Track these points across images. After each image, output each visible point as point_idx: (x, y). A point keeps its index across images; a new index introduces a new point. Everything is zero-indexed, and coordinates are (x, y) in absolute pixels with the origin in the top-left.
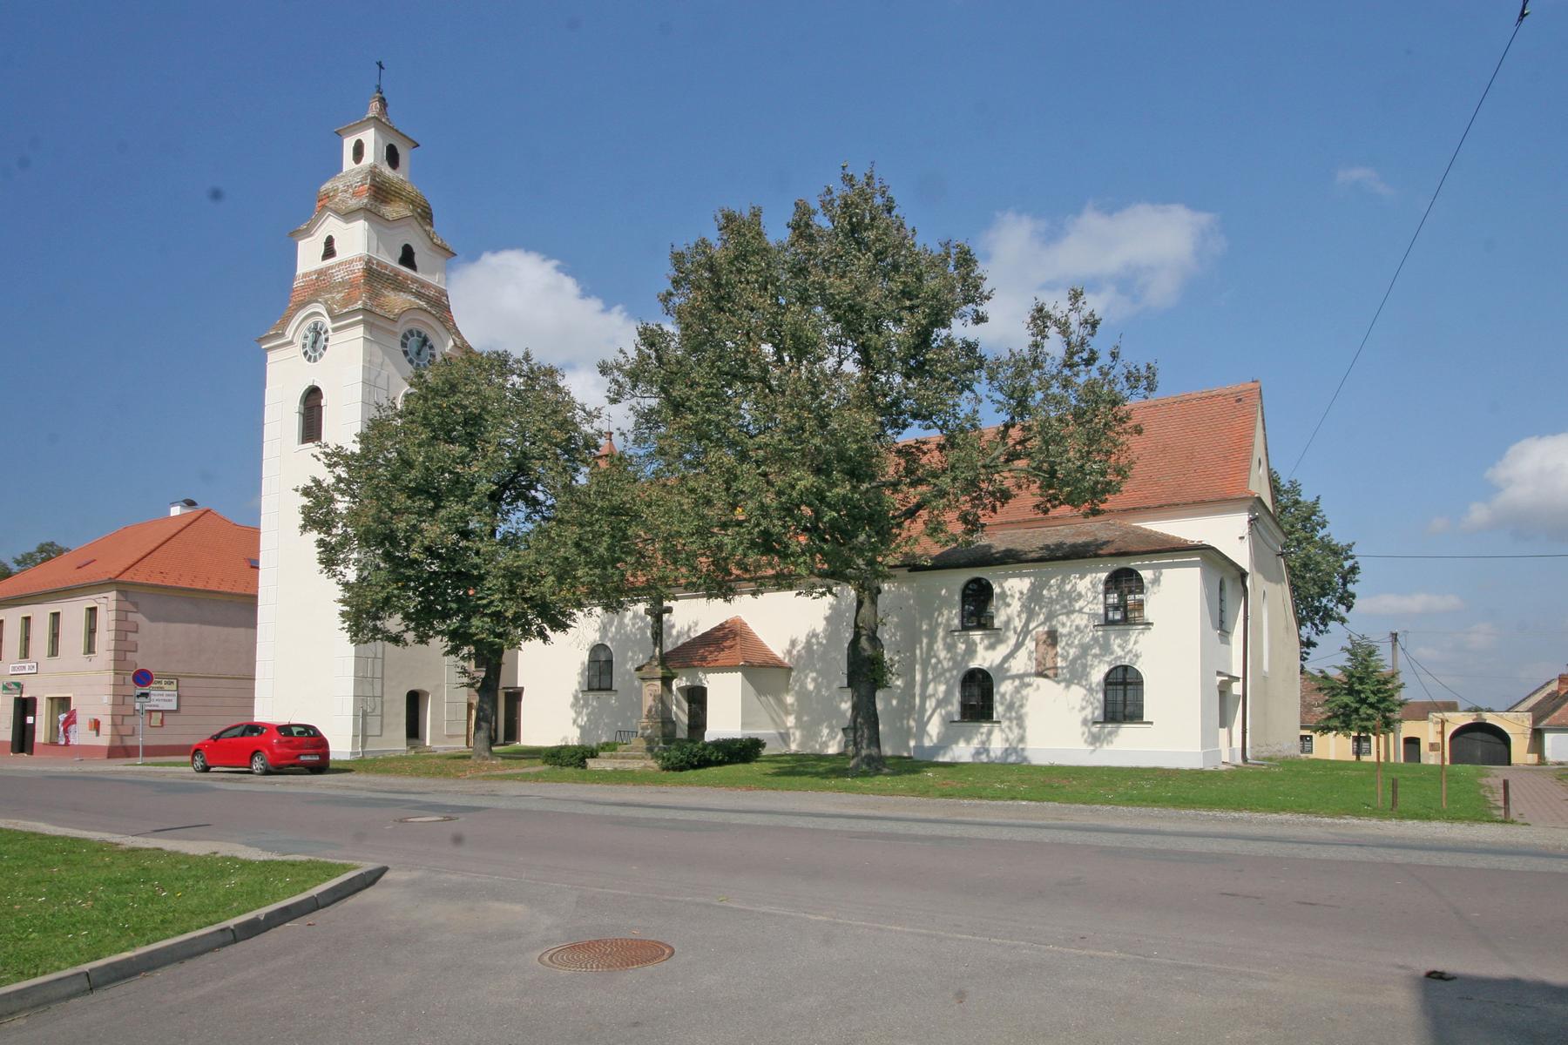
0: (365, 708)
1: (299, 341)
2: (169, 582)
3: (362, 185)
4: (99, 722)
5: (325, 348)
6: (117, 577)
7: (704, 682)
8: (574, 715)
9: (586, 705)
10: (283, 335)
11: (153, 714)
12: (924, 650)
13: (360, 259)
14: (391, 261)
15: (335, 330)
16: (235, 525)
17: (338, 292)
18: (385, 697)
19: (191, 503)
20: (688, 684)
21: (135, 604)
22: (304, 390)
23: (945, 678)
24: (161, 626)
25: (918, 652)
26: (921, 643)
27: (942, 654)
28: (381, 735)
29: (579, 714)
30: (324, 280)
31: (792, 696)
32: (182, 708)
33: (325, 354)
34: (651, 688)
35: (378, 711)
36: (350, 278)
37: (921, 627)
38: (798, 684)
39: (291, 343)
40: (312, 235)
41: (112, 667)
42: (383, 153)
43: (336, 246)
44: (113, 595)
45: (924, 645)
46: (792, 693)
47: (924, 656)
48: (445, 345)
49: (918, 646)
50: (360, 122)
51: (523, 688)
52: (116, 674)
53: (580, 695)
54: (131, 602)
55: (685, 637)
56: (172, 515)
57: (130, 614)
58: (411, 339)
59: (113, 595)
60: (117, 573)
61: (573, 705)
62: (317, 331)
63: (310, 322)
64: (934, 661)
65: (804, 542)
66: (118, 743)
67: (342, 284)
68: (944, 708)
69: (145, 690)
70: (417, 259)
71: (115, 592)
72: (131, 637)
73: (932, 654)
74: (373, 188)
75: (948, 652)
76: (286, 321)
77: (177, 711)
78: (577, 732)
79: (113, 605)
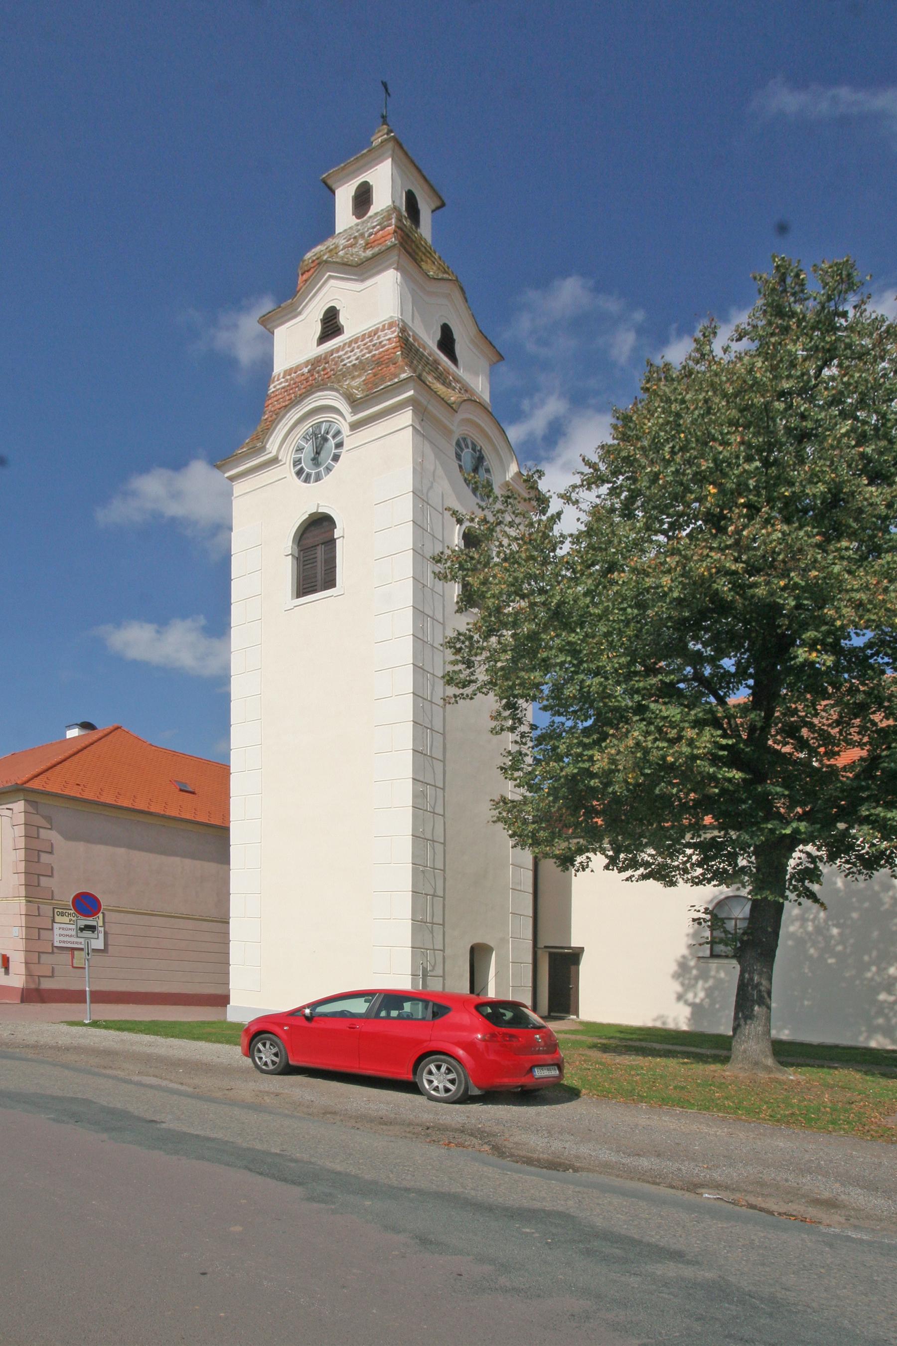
0: (425, 965)
1: (287, 457)
2: (89, 795)
3: (382, 229)
4: (8, 959)
5: (336, 458)
6: (25, 783)
8: (679, 988)
9: (704, 975)
10: (263, 449)
11: (76, 952)
13: (391, 325)
14: (430, 341)
15: (355, 426)
16: (151, 745)
17: (353, 378)
18: (448, 951)
19: (87, 726)
21: (49, 819)
22: (300, 521)
24: (80, 847)
29: (687, 987)
30: (324, 369)
32: (110, 947)
33: (337, 466)
35: (439, 971)
36: (374, 356)
39: (275, 461)
40: (300, 313)
41: (23, 893)
42: (401, 198)
43: (342, 319)
44: (19, 806)
48: (505, 470)
50: (369, 151)
51: (582, 950)
52: (28, 901)
53: (692, 963)
54: (42, 816)
56: (68, 737)
57: (41, 830)
58: (466, 450)
59: (19, 806)
60: (24, 779)
61: (676, 976)
62: (319, 440)
63: (307, 426)
65: (684, 821)
66: (33, 986)
67: (360, 366)
69: (90, 922)
70: (459, 349)
71: (23, 801)
72: (45, 858)
74: (399, 232)
76: (268, 431)
77: (105, 950)
78: (687, 1011)
79: (21, 818)
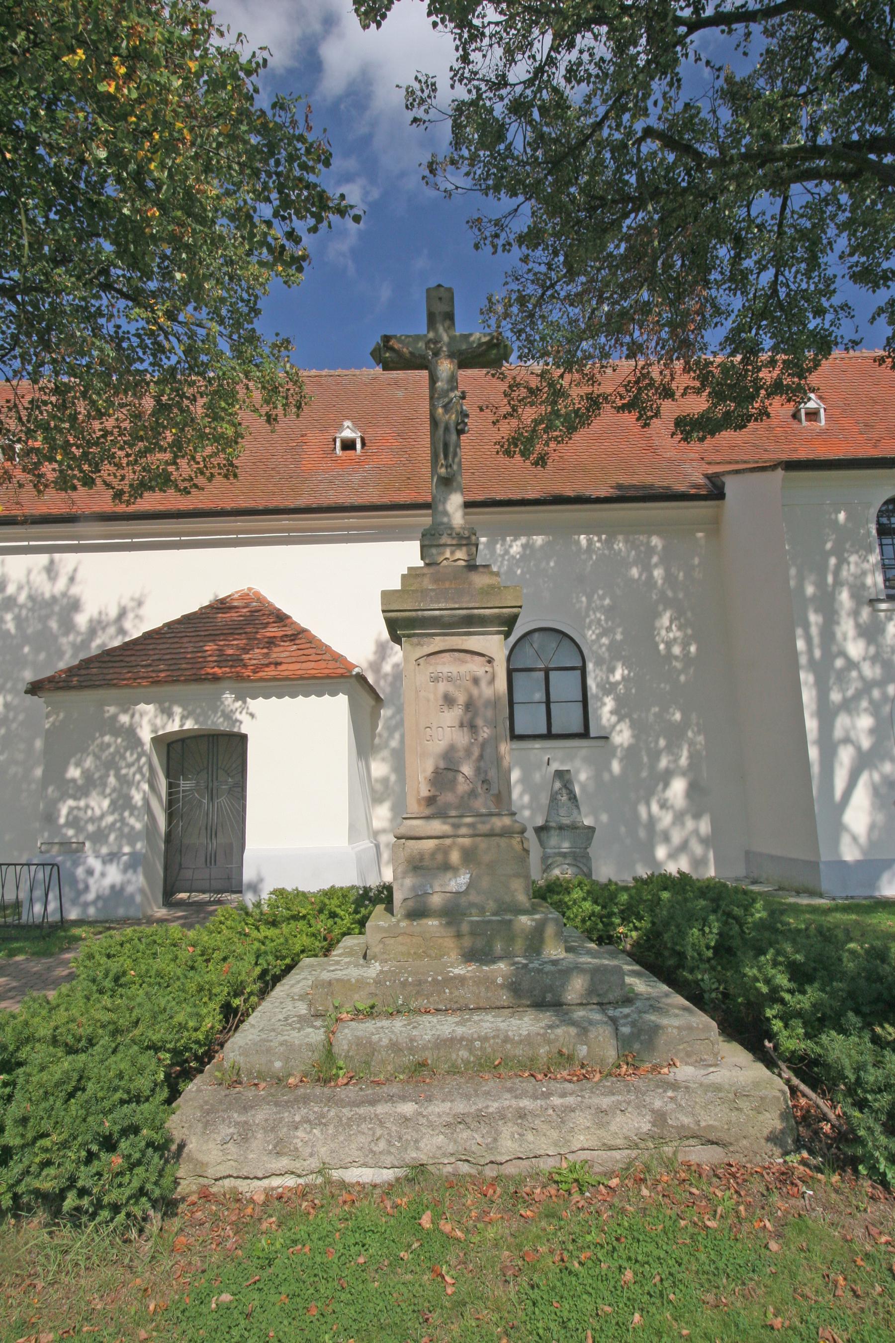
7: (243, 717)
12: (816, 640)
20: (189, 725)
23: (871, 701)
25: (801, 645)
26: (806, 626)
27: (855, 649)
28: (515, 737)
31: (383, 759)
34: (446, 666)
37: (801, 588)
38: (397, 736)
45: (814, 631)
46: (385, 753)
47: (817, 653)
49: (799, 631)
55: (112, 630)
64: (839, 663)
68: (876, 768)
73: (834, 649)
75: (869, 643)
